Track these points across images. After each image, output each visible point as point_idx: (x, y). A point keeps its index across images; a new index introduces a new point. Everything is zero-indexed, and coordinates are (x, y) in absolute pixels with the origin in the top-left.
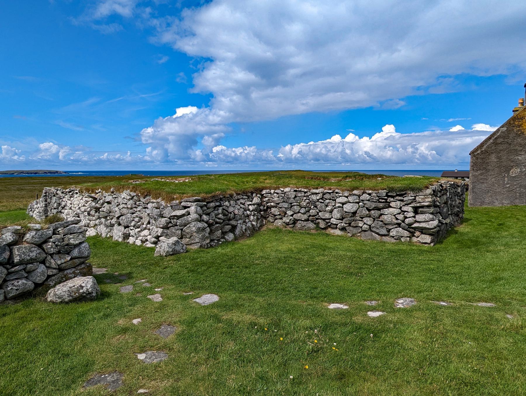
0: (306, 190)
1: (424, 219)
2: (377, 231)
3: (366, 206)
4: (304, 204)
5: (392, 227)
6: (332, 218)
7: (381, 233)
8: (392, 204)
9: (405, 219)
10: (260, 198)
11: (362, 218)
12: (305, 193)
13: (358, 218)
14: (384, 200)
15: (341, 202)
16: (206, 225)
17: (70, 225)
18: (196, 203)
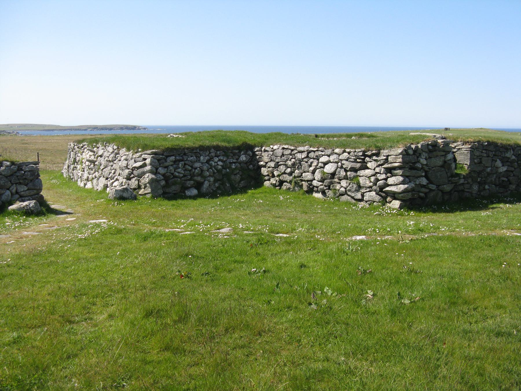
0: (292, 148)
1: (394, 182)
2: (353, 195)
3: (344, 166)
4: (289, 163)
5: (366, 191)
6: (314, 179)
7: (356, 198)
8: (369, 165)
9: (303, 173)
10: (250, 156)
11: (341, 180)
12: (292, 150)
13: (336, 180)
14: (360, 160)
15: (322, 161)
16: (162, 178)
17: (30, 164)
18: (152, 156)
